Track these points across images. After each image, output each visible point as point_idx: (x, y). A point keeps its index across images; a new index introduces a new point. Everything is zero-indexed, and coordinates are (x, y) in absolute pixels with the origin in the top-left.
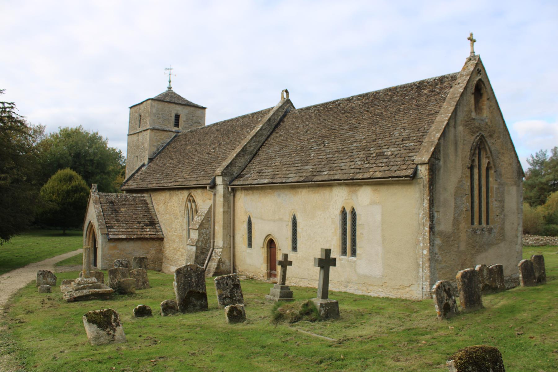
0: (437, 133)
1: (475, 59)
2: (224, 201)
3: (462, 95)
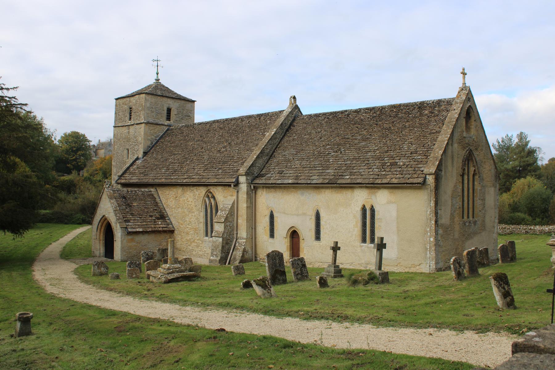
0: (440, 150)
1: (466, 89)
2: (247, 198)
3: (457, 120)
